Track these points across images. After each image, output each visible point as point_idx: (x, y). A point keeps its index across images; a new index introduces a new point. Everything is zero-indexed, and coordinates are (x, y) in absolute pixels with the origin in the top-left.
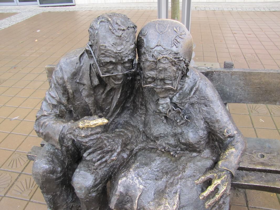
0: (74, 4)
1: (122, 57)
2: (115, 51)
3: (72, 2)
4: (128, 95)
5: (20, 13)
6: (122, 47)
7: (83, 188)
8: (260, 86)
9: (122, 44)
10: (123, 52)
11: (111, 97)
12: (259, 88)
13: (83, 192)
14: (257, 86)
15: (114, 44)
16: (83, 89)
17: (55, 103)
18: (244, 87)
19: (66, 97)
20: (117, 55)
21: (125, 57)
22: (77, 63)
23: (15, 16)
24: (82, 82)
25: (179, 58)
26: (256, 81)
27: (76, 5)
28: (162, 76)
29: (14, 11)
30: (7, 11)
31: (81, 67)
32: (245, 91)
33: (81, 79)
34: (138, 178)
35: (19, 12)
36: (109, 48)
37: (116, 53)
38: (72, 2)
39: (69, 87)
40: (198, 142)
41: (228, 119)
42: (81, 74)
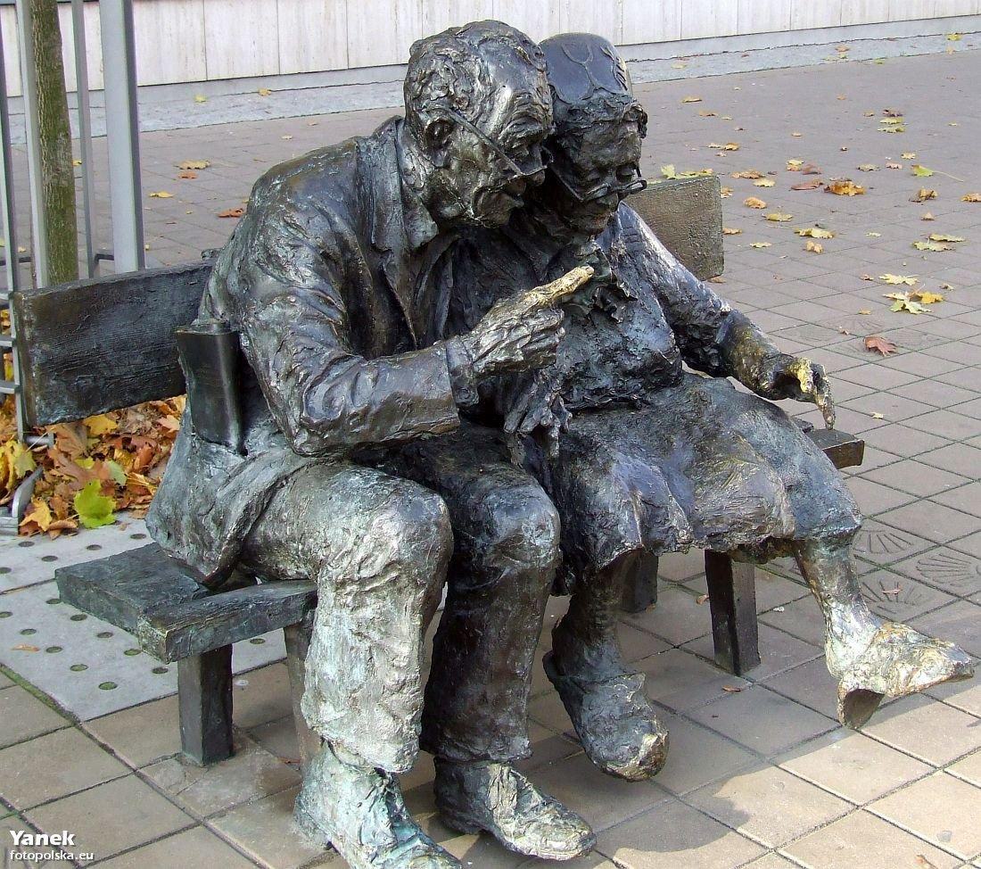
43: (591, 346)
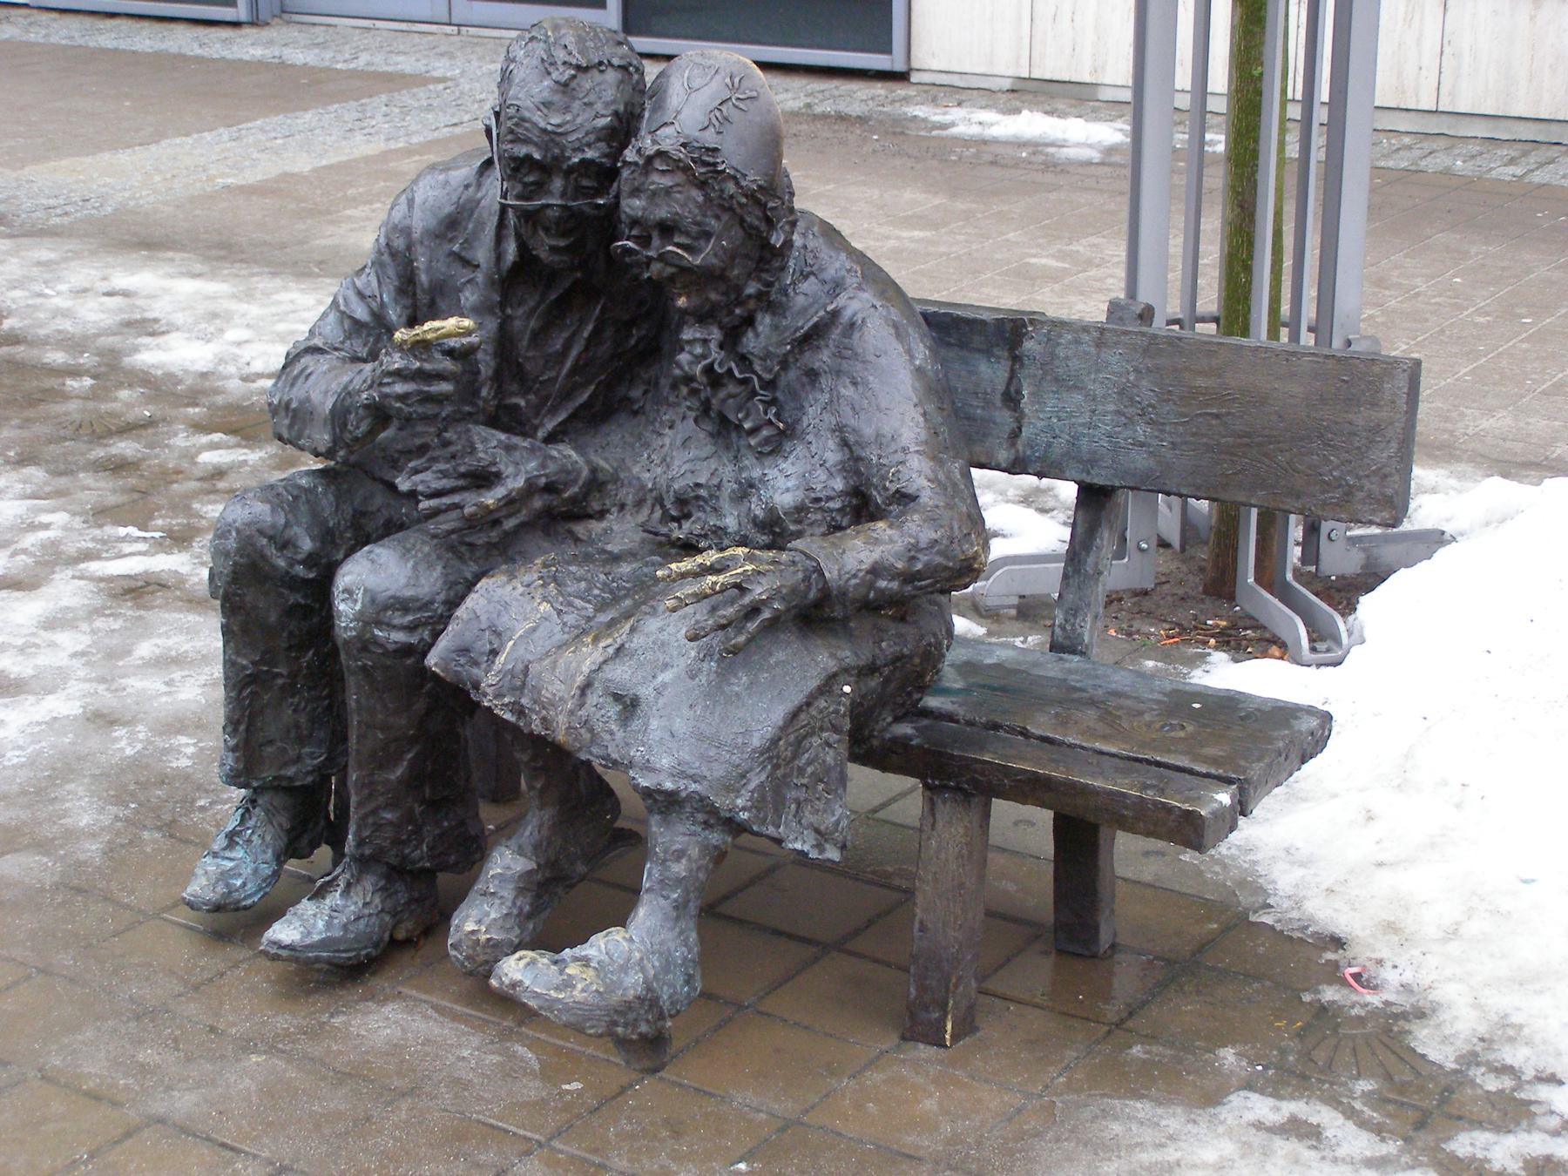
0: (899, 66)
1: (563, 149)
2: (542, 124)
3: (887, 49)
4: (633, 342)
6: (568, 117)
9: (567, 109)
12: (1217, 416)
13: (358, 607)
14: (1207, 406)
15: (547, 105)
17: (361, 313)
18: (1154, 407)
19: (405, 307)
20: (550, 137)
21: (574, 150)
22: (467, 187)
23: (405, 98)
24: (467, 255)
25: (715, 164)
27: (915, 78)
28: (662, 213)
31: (479, 202)
32: (1162, 431)
34: (541, 578)
36: (527, 114)
37: (544, 131)
38: (887, 49)
39: (421, 262)
41: (923, 436)
42: (470, 226)
43: (728, 472)
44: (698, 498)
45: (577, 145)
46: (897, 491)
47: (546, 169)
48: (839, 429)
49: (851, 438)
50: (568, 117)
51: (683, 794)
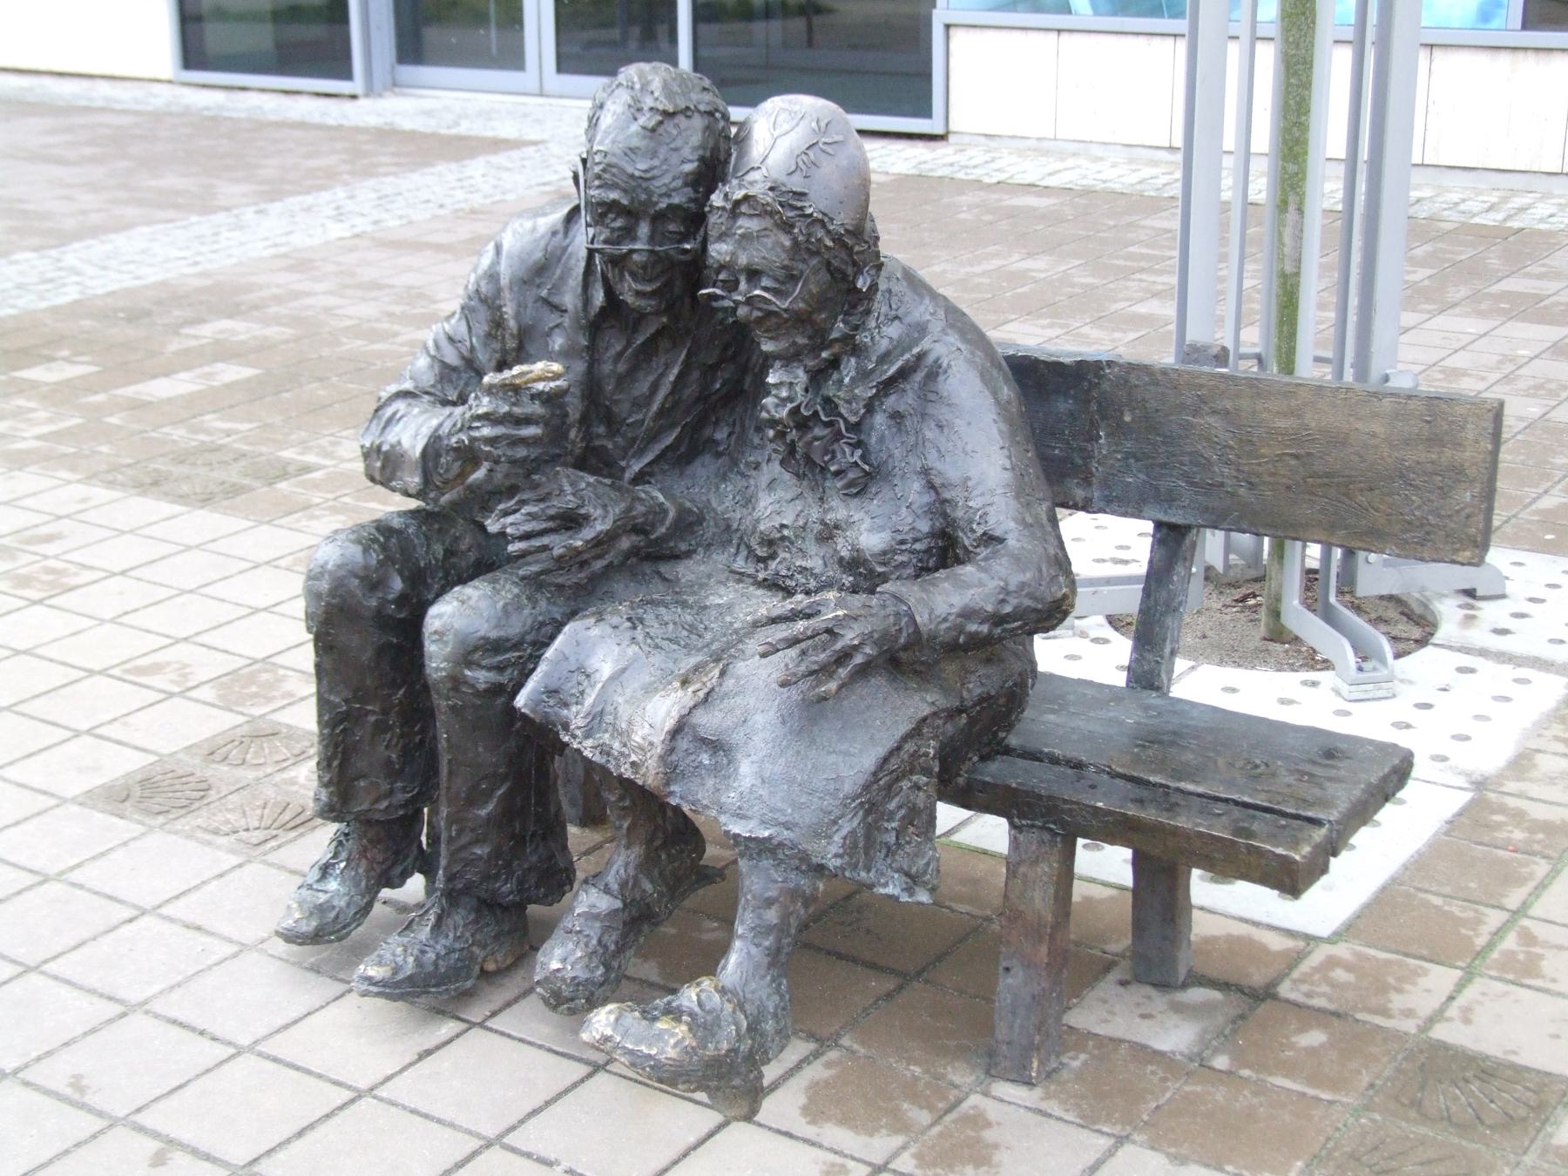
0: (939, 130)
1: (649, 193)
3: (925, 111)
5: (534, 143)
6: (656, 162)
7: (450, 637)
8: (1302, 452)
10: (653, 178)
11: (651, 378)
12: (1296, 457)
16: (557, 326)
23: (500, 159)
24: (555, 300)
25: (801, 208)
26: (1282, 423)
27: (951, 138)
29: (507, 130)
30: (457, 124)
33: (556, 289)
35: (532, 137)
37: (632, 176)
38: (925, 111)
39: (509, 310)
40: (884, 553)
44: (783, 538)
45: (664, 190)
46: (985, 534)
47: (631, 214)
48: (925, 472)
49: (937, 481)
50: (656, 162)
51: (775, 842)
